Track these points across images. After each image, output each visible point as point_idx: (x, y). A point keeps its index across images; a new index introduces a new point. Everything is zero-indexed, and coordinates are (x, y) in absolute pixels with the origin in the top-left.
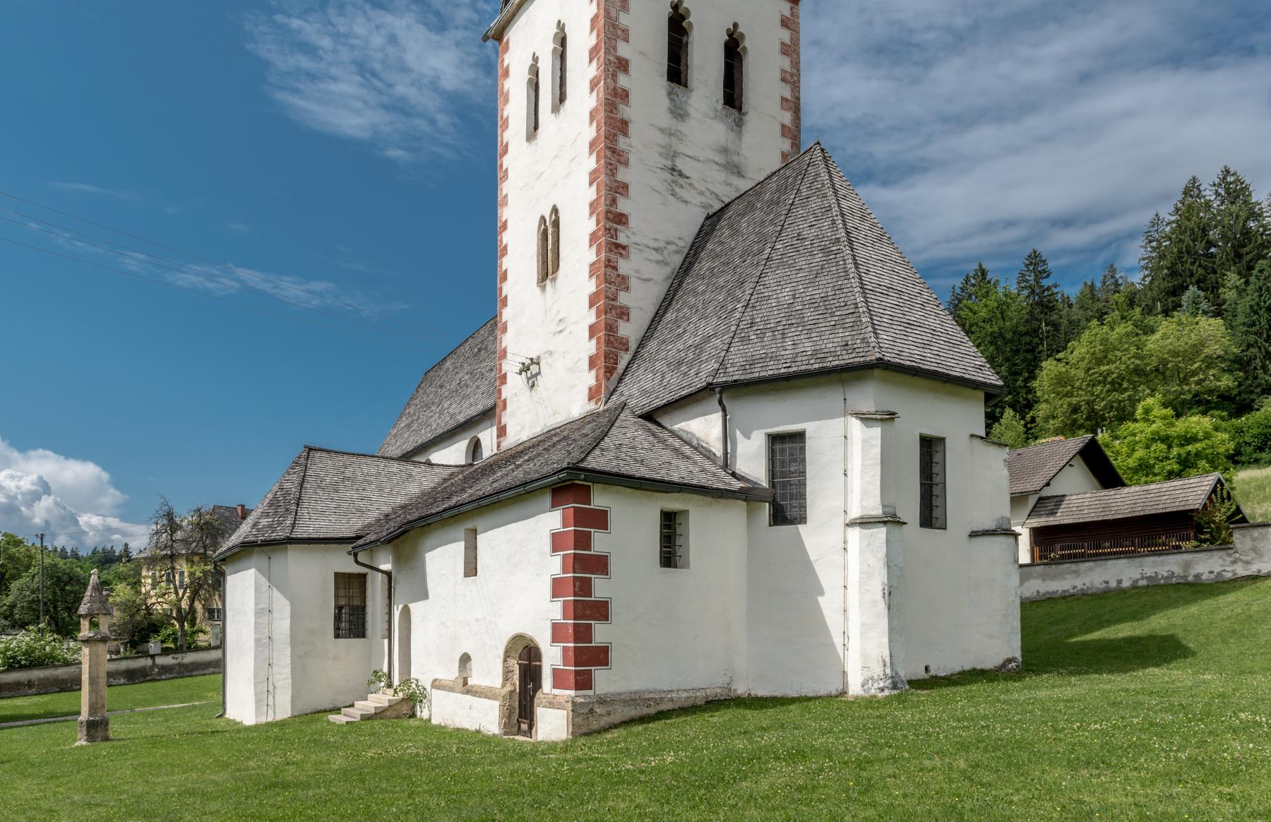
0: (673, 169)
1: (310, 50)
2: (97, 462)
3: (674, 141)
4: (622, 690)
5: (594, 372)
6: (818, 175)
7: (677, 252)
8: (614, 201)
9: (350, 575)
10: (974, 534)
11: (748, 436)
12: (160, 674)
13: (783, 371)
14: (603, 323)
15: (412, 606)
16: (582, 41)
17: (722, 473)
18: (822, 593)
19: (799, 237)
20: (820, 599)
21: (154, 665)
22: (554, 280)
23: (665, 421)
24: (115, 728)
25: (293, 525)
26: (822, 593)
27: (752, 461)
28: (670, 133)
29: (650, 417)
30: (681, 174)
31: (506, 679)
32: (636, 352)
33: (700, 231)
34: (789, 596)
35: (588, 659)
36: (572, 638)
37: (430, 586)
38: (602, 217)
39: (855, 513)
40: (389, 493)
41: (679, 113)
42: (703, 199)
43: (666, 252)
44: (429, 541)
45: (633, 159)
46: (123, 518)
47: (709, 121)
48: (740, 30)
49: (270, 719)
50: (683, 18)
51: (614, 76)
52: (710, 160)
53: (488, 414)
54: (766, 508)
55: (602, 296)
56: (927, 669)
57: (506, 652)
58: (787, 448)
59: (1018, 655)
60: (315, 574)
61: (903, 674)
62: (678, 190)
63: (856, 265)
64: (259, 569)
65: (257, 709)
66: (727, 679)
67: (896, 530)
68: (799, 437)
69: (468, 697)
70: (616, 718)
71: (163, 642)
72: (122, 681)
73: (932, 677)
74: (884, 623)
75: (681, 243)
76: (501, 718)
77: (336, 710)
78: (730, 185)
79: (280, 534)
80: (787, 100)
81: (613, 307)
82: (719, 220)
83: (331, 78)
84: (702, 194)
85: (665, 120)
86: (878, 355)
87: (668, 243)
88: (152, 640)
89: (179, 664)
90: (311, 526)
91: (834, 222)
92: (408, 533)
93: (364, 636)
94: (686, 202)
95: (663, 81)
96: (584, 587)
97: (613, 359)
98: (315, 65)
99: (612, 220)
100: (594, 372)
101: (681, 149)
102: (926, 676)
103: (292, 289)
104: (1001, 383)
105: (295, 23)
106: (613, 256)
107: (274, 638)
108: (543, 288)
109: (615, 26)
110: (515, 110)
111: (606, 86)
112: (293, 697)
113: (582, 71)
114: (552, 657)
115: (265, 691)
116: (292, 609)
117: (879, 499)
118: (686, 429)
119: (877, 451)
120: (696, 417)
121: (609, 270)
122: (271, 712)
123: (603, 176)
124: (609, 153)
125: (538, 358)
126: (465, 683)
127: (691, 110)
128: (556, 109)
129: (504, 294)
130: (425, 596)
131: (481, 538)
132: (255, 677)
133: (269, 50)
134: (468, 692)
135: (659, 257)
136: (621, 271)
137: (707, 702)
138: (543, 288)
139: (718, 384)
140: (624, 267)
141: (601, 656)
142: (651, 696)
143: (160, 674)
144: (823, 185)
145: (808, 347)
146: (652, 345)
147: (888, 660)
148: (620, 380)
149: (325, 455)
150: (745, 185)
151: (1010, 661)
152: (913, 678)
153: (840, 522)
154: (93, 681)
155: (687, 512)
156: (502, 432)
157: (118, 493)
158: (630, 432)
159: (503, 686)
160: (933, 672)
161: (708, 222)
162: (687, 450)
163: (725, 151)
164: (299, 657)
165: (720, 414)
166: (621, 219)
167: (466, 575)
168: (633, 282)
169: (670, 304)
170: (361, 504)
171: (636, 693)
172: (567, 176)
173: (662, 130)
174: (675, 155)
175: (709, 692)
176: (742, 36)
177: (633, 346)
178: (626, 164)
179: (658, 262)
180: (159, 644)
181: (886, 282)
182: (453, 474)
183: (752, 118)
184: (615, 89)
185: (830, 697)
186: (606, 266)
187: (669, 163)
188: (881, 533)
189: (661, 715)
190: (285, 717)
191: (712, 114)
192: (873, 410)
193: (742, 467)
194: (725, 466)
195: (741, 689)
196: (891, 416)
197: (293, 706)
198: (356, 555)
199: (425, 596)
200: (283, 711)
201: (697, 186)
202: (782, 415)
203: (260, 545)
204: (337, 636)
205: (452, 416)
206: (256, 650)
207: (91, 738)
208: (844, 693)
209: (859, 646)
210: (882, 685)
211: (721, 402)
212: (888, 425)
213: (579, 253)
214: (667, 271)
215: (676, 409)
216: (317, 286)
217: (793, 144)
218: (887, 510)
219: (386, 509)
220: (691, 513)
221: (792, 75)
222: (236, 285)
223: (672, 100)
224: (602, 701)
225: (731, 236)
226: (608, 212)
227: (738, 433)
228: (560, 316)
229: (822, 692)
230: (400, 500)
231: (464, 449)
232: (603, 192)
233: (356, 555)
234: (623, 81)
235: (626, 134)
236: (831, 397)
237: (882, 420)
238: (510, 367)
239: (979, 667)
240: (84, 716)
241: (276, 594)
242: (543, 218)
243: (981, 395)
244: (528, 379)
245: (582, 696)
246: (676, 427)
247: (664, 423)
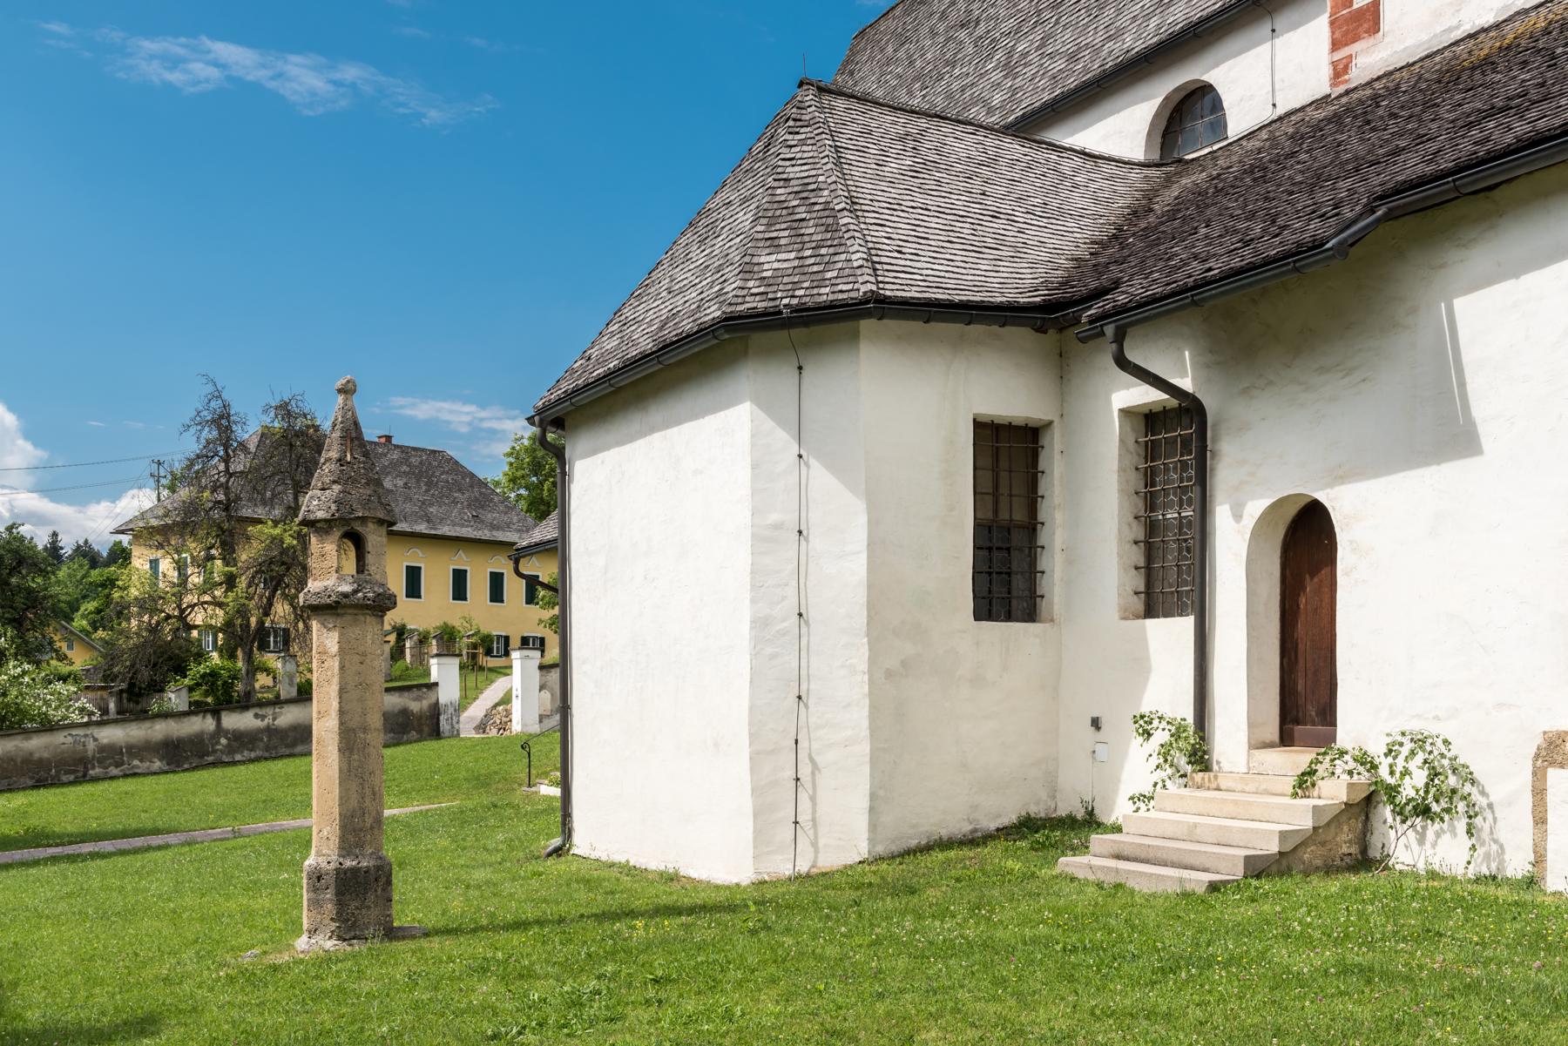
12: (230, 750)
21: (219, 729)
24: (412, 902)
37: (1479, 411)
44: (1479, 255)
46: (43, 490)
49: (803, 867)
60: (915, 414)
64: (757, 401)
65: (761, 837)
71: (191, 689)
72: (157, 765)
89: (268, 729)
93: (1030, 614)
103: (304, 78)
107: (812, 614)
112: (873, 797)
116: (873, 524)
122: (803, 843)
132: (753, 737)
143: (230, 750)
154: (350, 740)
157: (29, 446)
164: (889, 674)
180: (184, 693)
190: (853, 857)
197: (873, 827)
200: (843, 837)
206: (755, 655)
207: (348, 929)
216: (350, 72)
222: (214, 73)
233: (517, 562)
240: (323, 852)
241: (820, 476)
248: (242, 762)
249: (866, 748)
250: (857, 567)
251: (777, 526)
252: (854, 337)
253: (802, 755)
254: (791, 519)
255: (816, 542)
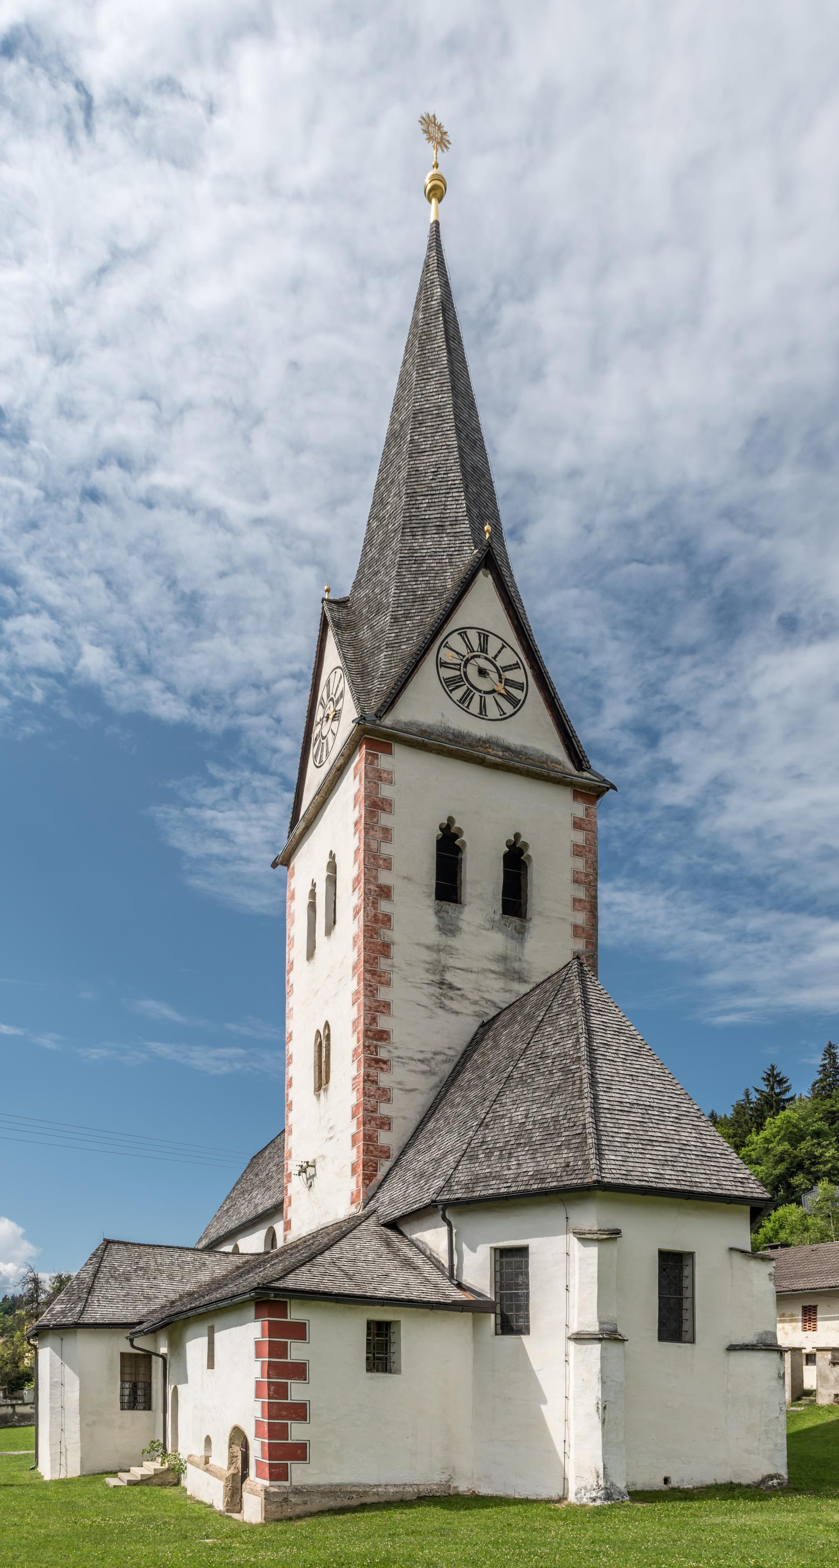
0: (442, 983)
1: (223, 835)
2: (12, 1219)
3: (443, 956)
4: (322, 1482)
5: (355, 1178)
6: (571, 991)
7: (445, 1062)
8: (374, 1020)
9: (130, 1354)
10: (732, 1348)
11: (474, 1250)
12: (19, 1421)
13: (502, 1190)
14: (361, 1134)
15: (179, 1387)
16: (349, 870)
17: (445, 1283)
18: (545, 1402)
19: (543, 1056)
20: (543, 1407)
21: (14, 1413)
22: (326, 1090)
23: (405, 1229)
25: (82, 1312)
26: (545, 1402)
27: (478, 1272)
28: (438, 949)
29: (393, 1225)
30: (451, 987)
31: (231, 1463)
32: (398, 1159)
33: (473, 1039)
34: (511, 1402)
35: (285, 1453)
36: (267, 1435)
38: (361, 1035)
39: (575, 1328)
40: (181, 1281)
41: (448, 928)
42: (477, 1008)
43: (433, 1063)
45: (395, 978)
47: (484, 932)
48: (522, 839)
49: (62, 1476)
50: (456, 836)
51: (375, 904)
52: (484, 971)
53: (277, 1210)
54: (492, 1320)
55: (361, 1109)
56: (666, 1480)
57: (230, 1439)
58: (511, 1262)
59: (783, 1472)
60: (102, 1355)
61: (621, 1485)
62: (447, 1002)
63: (593, 1083)
64: (53, 1349)
66: (445, 1477)
67: (615, 1349)
68: (523, 1251)
69: (207, 1474)
70: (314, 1507)
73: (673, 1489)
74: (598, 1434)
75: (450, 1053)
76: (226, 1496)
77: (114, 1473)
78: (510, 991)
79: (70, 1320)
80: (580, 901)
81: (374, 1119)
82: (489, 1030)
83: (242, 859)
84: (475, 1003)
85: (434, 937)
86: (595, 1178)
87: (435, 1054)
88: (27, 1388)
90: (99, 1312)
91: (578, 1039)
92: (175, 1323)
94: (457, 1013)
95: (429, 902)
96: (280, 1391)
97: (376, 1164)
98: (227, 849)
99: (374, 1037)
100: (355, 1178)
101: (451, 962)
102: (664, 1487)
103: (201, 1058)
104: (767, 1195)
105: (209, 814)
106: (372, 1071)
107: (65, 1407)
108: (318, 1096)
109: (375, 857)
110: (297, 930)
111: (366, 915)
112: (82, 1458)
113: (350, 899)
114: (256, 1449)
115: (60, 1452)
116: (81, 1384)
117: (596, 1316)
118: (421, 1239)
119: (594, 1269)
120: (429, 1229)
121: (368, 1084)
122: (63, 1470)
123: (362, 998)
124: (368, 976)
125: (314, 1161)
126: (207, 1462)
127: (463, 925)
128: (328, 932)
129: (290, 1099)
130: (185, 1381)
131: (217, 1336)
132: (50, 1440)
133: (181, 840)
134: (207, 1470)
135: (424, 1067)
136: (381, 1085)
137: (402, 1501)
138: (318, 1096)
139: (441, 1201)
140: (384, 1080)
141: (300, 1452)
142: (354, 1489)
143: (19, 1421)
144: (574, 1002)
145: (530, 1168)
146: (411, 1153)
147: (601, 1472)
148: (380, 1186)
149: (122, 1247)
150: (525, 988)
151: (771, 1477)
152: (639, 1488)
153: (562, 1335)
155: (399, 1321)
156: (288, 1226)
158: (367, 1243)
159: (229, 1469)
160: (674, 1483)
161: (481, 1030)
162: (419, 1260)
163: (503, 959)
164: (87, 1425)
165: (444, 1230)
166: (382, 1036)
167: (208, 1368)
168: (396, 1094)
169: (433, 1113)
170: (151, 1292)
171: (337, 1485)
172: (336, 994)
173: (428, 948)
174: (445, 969)
175: (421, 1488)
176: (526, 845)
177: (395, 1153)
178: (388, 983)
179: (424, 1073)
181: (632, 1098)
182: (247, 1262)
183: (537, 926)
184: (375, 915)
185: (548, 1501)
186: (365, 1081)
187: (437, 978)
188: (596, 1349)
189: (363, 1507)
191: (488, 926)
192: (596, 1228)
193: (468, 1278)
194: (451, 1277)
195: (463, 1486)
196: (615, 1233)
197: (82, 1467)
198: (131, 1341)
199: (185, 1381)
200: (74, 1470)
201: (470, 996)
202: (507, 1231)
203: (52, 1329)
204: (122, 1409)
205: (256, 1205)
206: (51, 1417)
208: (562, 1499)
209: (577, 1456)
210: (594, 1494)
211: (444, 1218)
212: (607, 1247)
213: (346, 1067)
214: (434, 1080)
215: (414, 1220)
217: (587, 943)
218: (605, 1326)
219: (173, 1296)
220: (402, 1322)
221: (587, 875)
223: (440, 917)
224: (297, 1491)
225: (492, 1048)
226: (366, 1031)
227: (464, 1246)
228: (331, 1125)
229: (544, 1495)
230: (189, 1288)
231: (263, 1237)
232: (362, 1012)
233: (131, 1341)
234: (384, 907)
235: (387, 956)
236: (555, 1215)
237: (598, 1240)
238: (292, 1166)
239: (735, 1481)
241: (67, 1370)
242: (318, 1032)
243: (747, 1209)
244: (308, 1179)
245: (275, 1487)
246: (414, 1237)
247: (405, 1232)
248: (24, 1426)
249: (79, 1445)
250: (76, 1395)
251: (56, 1382)
252: (76, 1332)
253: (63, 1446)
254: (59, 1380)
255: (67, 1388)
